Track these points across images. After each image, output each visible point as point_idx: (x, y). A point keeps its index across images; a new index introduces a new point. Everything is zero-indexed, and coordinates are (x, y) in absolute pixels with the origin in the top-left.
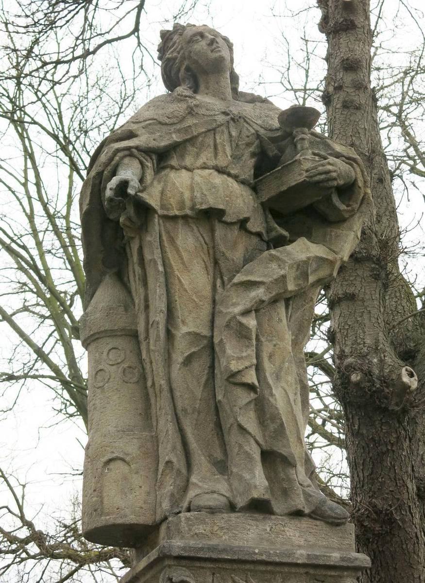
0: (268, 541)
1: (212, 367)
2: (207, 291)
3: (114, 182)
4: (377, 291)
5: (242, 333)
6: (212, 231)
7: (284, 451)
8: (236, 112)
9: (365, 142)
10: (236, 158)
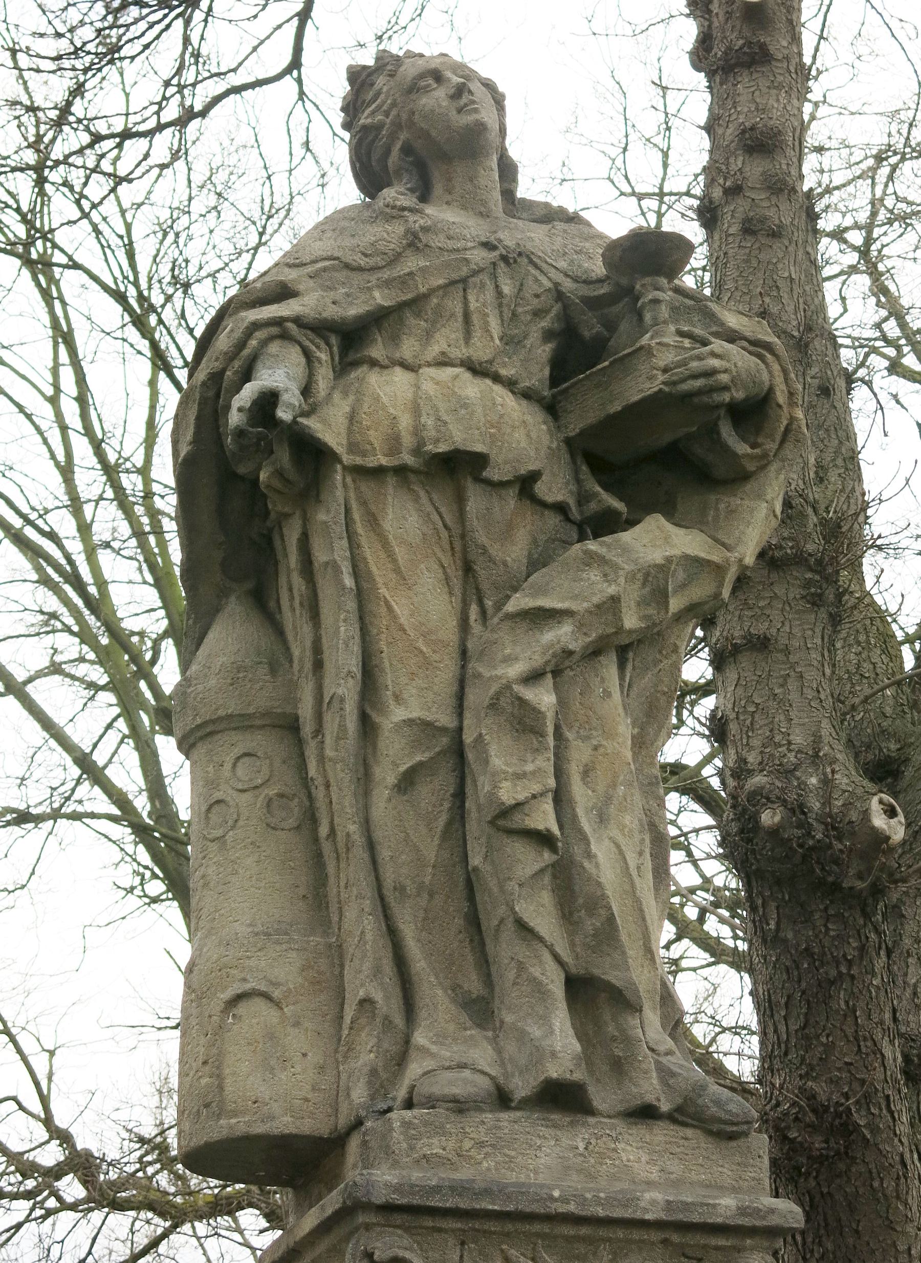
0: (580, 1171)
1: (460, 795)
2: (449, 631)
3: (247, 393)
4: (818, 630)
5: (525, 722)
6: (460, 500)
7: (614, 977)
8: (511, 243)
9: (790, 308)
10: (511, 342)
